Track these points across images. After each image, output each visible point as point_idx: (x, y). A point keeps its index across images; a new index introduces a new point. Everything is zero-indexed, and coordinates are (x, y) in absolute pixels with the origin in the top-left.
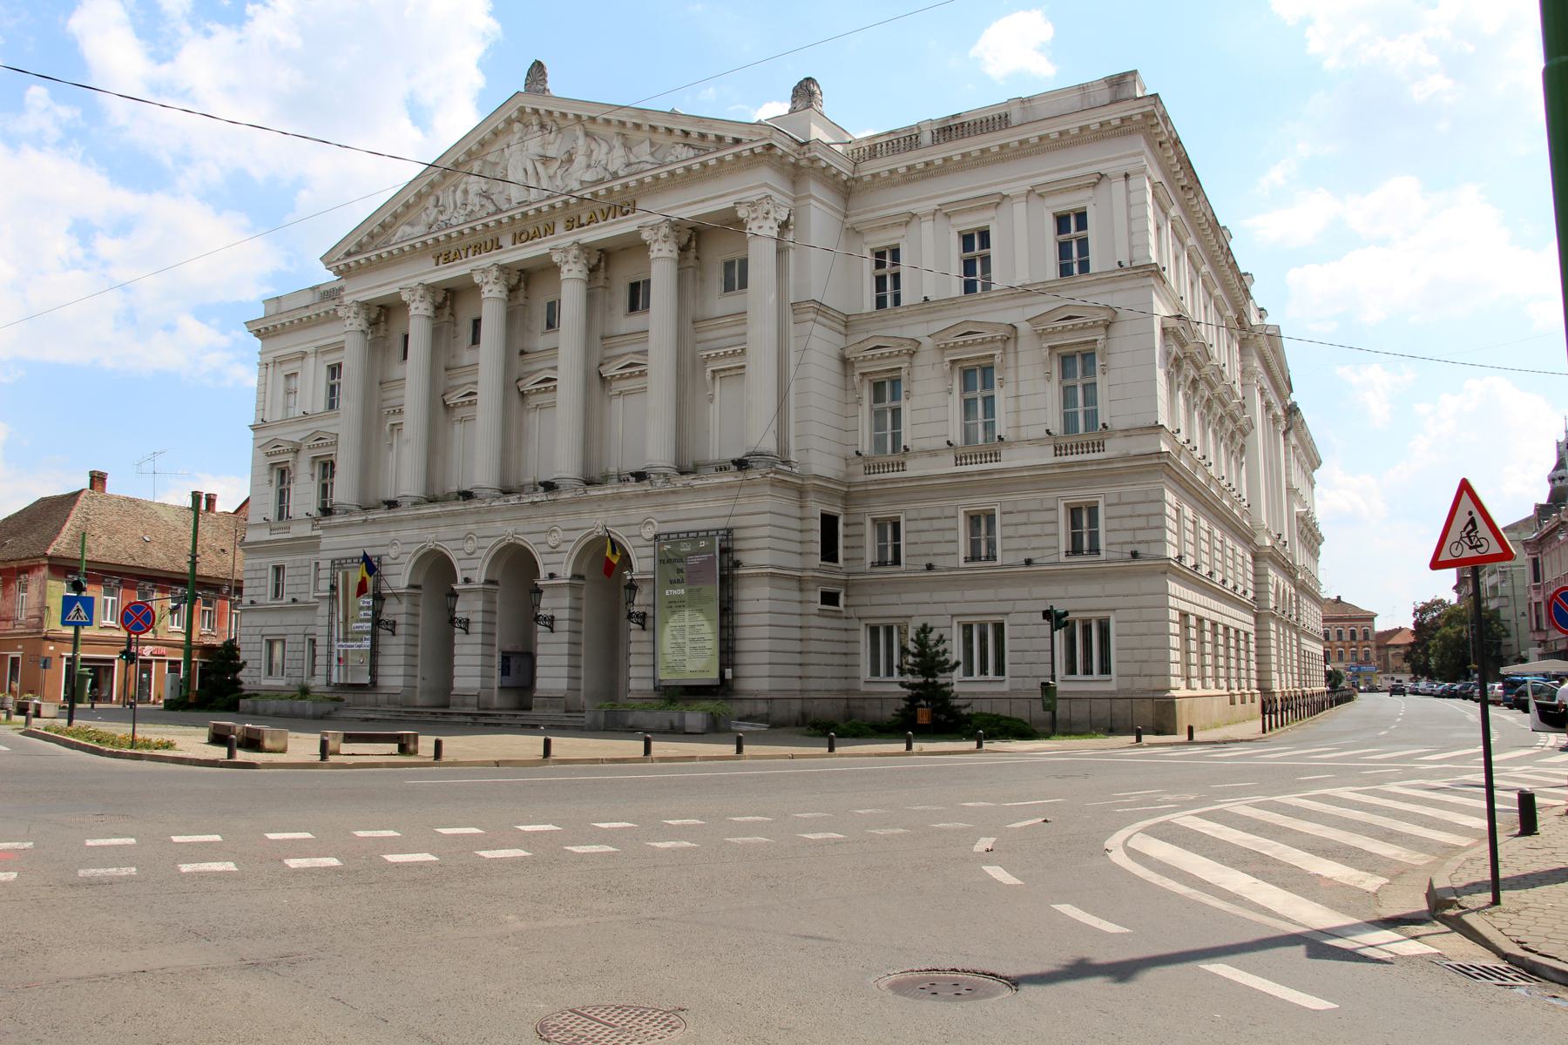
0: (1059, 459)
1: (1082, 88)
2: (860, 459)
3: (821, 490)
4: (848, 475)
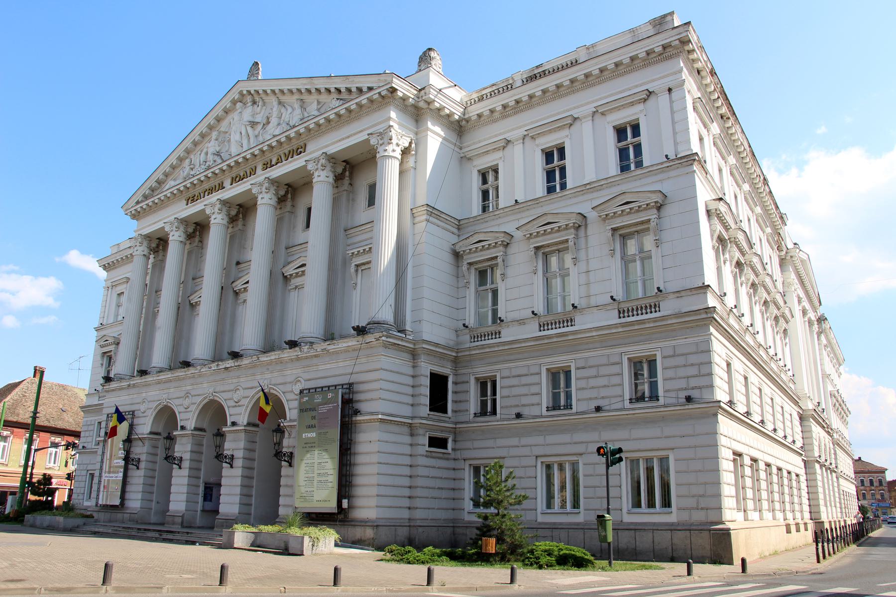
0: (623, 320)
1: (632, 31)
2: (467, 331)
3: (430, 353)
4: (458, 343)
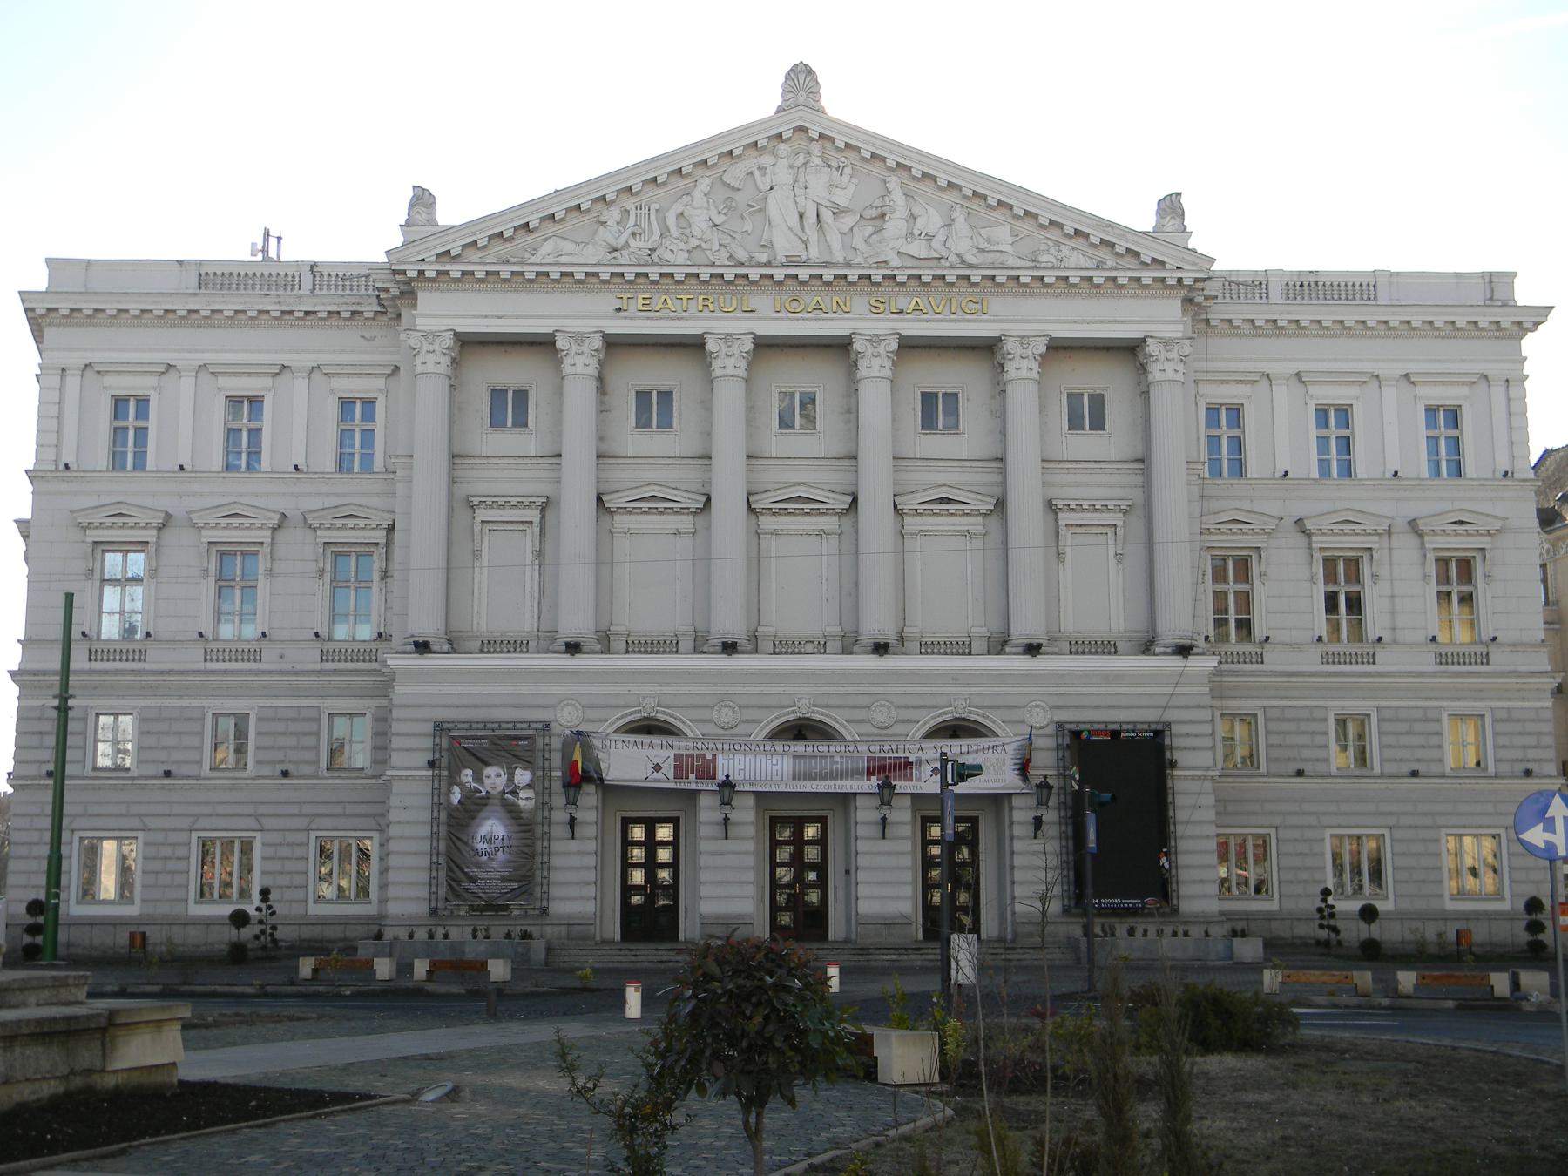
0: (1443, 668)
